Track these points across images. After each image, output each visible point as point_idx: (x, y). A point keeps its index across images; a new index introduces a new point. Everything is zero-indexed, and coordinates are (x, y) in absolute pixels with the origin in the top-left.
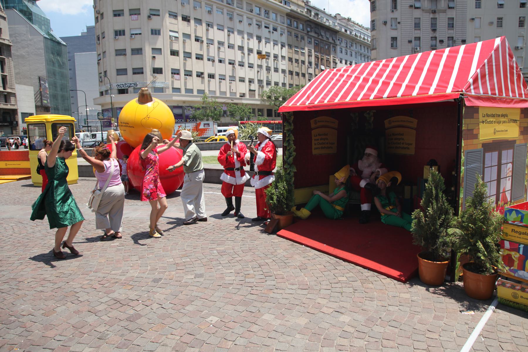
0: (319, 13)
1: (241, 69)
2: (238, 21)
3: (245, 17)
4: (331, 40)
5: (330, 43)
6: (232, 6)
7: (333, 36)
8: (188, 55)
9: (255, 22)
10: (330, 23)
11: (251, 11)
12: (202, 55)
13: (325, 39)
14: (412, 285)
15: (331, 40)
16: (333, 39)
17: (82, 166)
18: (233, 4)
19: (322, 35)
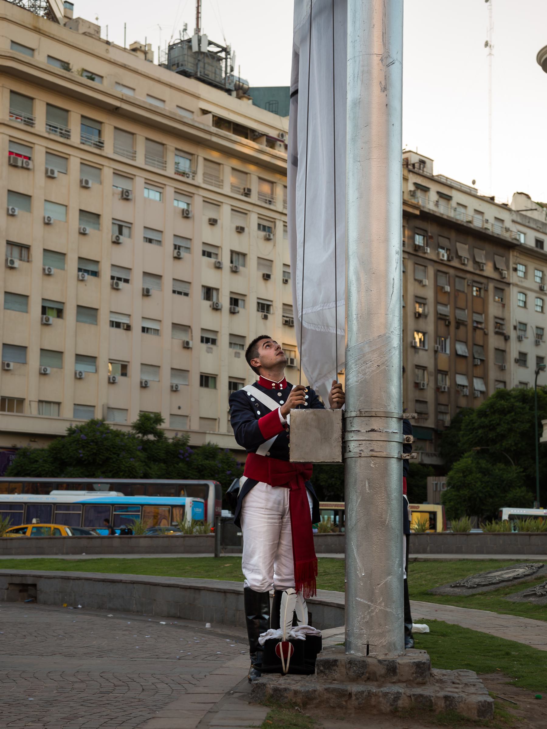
0: (454, 194)
1: (209, 351)
2: (205, 219)
3: (226, 210)
4: (489, 270)
5: (487, 278)
6: (189, 181)
7: (497, 258)
8: (52, 310)
9: (253, 220)
10: (488, 221)
11: (247, 193)
12: (172, 375)
13: (470, 267)
14: (209, 444)
15: (489, 270)
16: (496, 269)
17: (61, 269)
18: (195, 173)
19: (460, 257)
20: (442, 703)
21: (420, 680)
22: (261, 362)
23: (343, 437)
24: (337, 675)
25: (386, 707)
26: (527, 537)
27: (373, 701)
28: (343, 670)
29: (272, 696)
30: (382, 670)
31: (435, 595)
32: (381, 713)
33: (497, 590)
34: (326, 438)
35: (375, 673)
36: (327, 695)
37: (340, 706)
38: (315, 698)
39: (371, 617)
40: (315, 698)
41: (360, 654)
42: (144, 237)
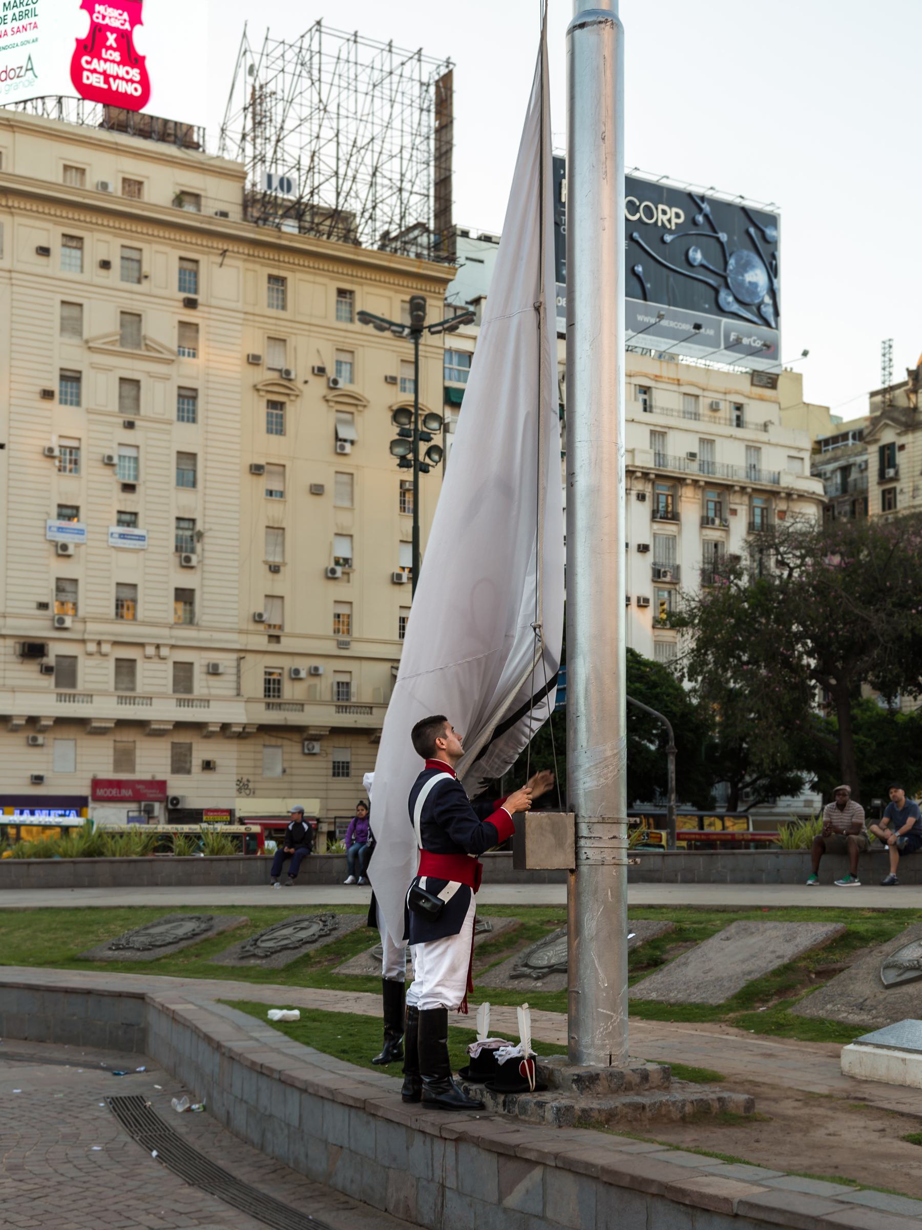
20: (716, 1105)
21: (666, 1084)
22: (448, 745)
23: (576, 842)
24: (600, 1089)
25: (676, 1115)
26: (25, 867)
27: (663, 1111)
28: (606, 1083)
29: (580, 1117)
30: (636, 1079)
31: (93, 961)
32: (672, 1121)
33: (181, 952)
34: (560, 844)
35: (630, 1083)
36: (625, 1110)
37: (636, 1120)
38: (616, 1115)
39: (614, 1028)
40: (616, 1115)
41: (602, 1065)
42: (266, 562)
